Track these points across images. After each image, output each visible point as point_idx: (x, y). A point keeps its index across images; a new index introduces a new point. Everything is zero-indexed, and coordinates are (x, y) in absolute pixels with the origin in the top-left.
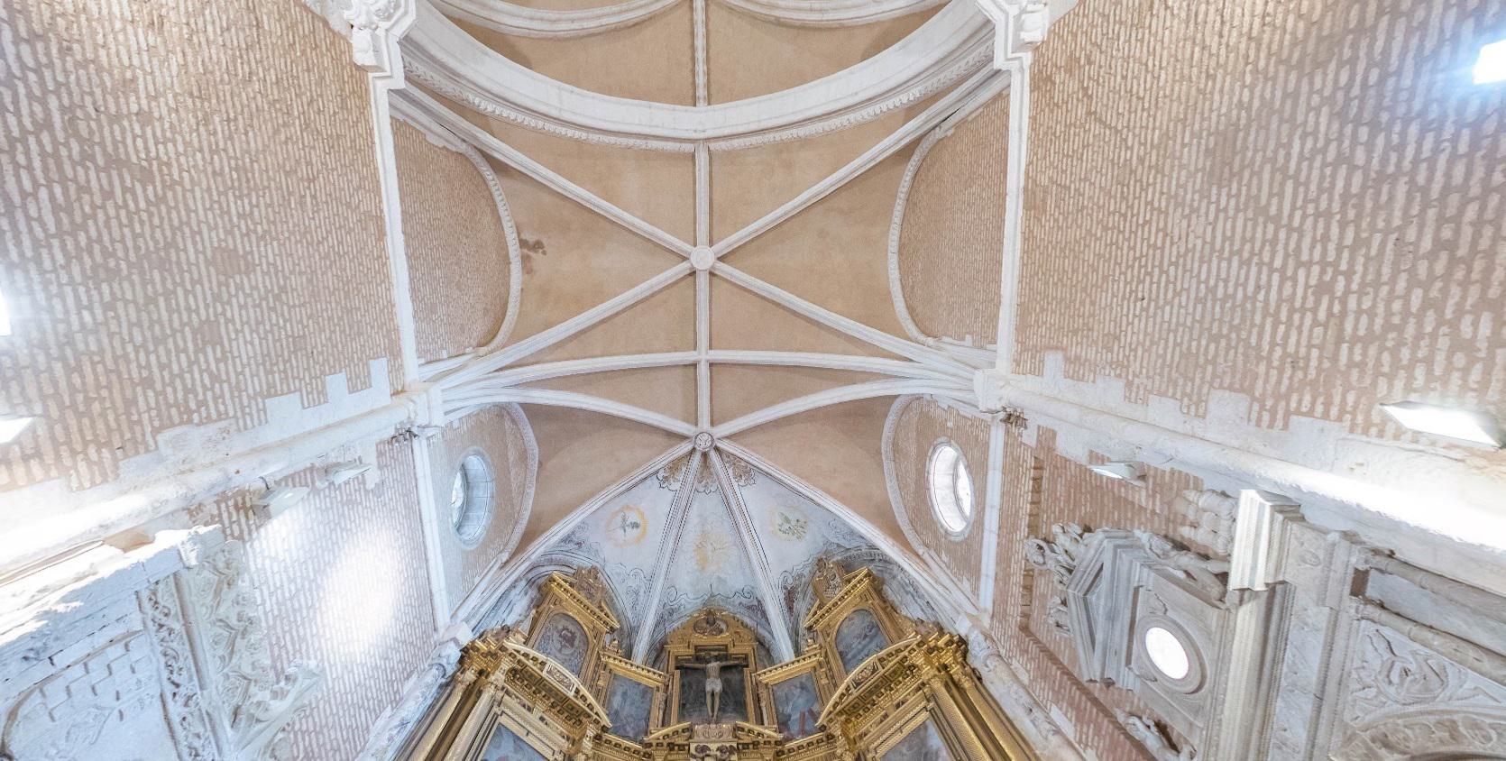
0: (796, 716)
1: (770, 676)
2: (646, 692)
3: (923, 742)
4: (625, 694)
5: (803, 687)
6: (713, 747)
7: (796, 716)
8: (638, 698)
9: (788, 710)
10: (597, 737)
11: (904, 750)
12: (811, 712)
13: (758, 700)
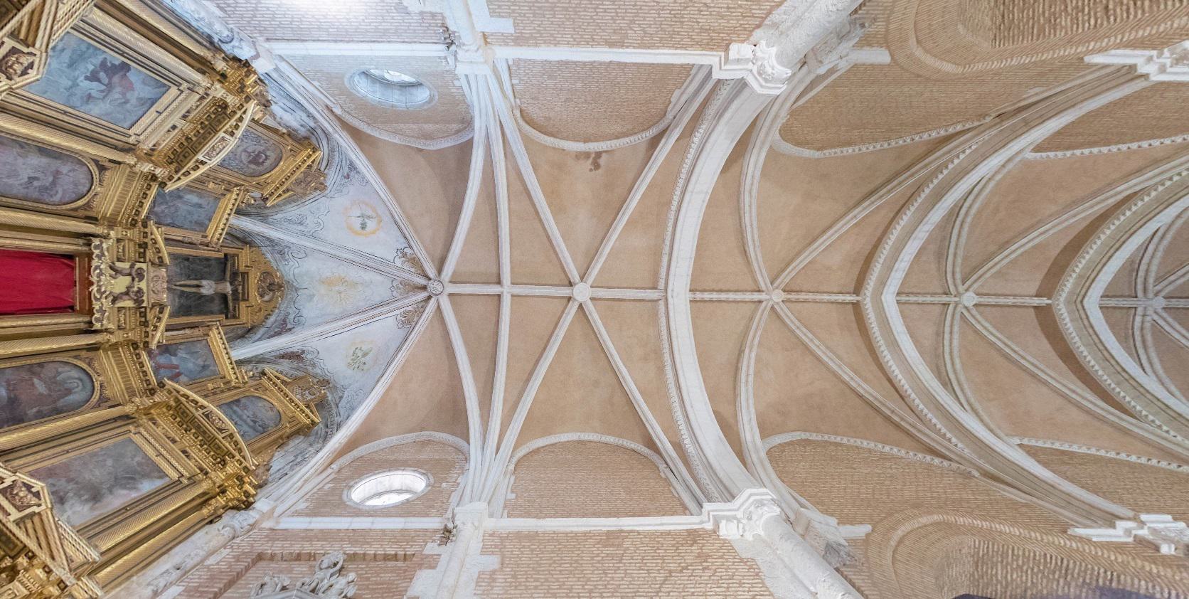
0: (174, 361)
1: (216, 338)
2: (202, 226)
3: (146, 476)
4: (200, 206)
5: (204, 367)
6: (143, 285)
7: (174, 361)
8: (195, 217)
9: (182, 354)
10: (154, 178)
11: (137, 459)
12: (179, 374)
13: (193, 326)
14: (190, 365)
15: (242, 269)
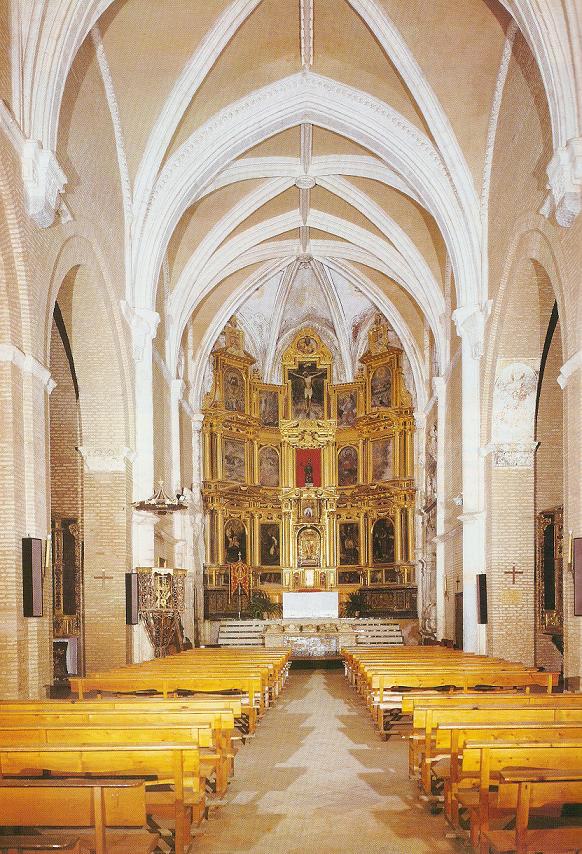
5: (352, 397)
9: (343, 408)
14: (349, 406)
15: (296, 368)
